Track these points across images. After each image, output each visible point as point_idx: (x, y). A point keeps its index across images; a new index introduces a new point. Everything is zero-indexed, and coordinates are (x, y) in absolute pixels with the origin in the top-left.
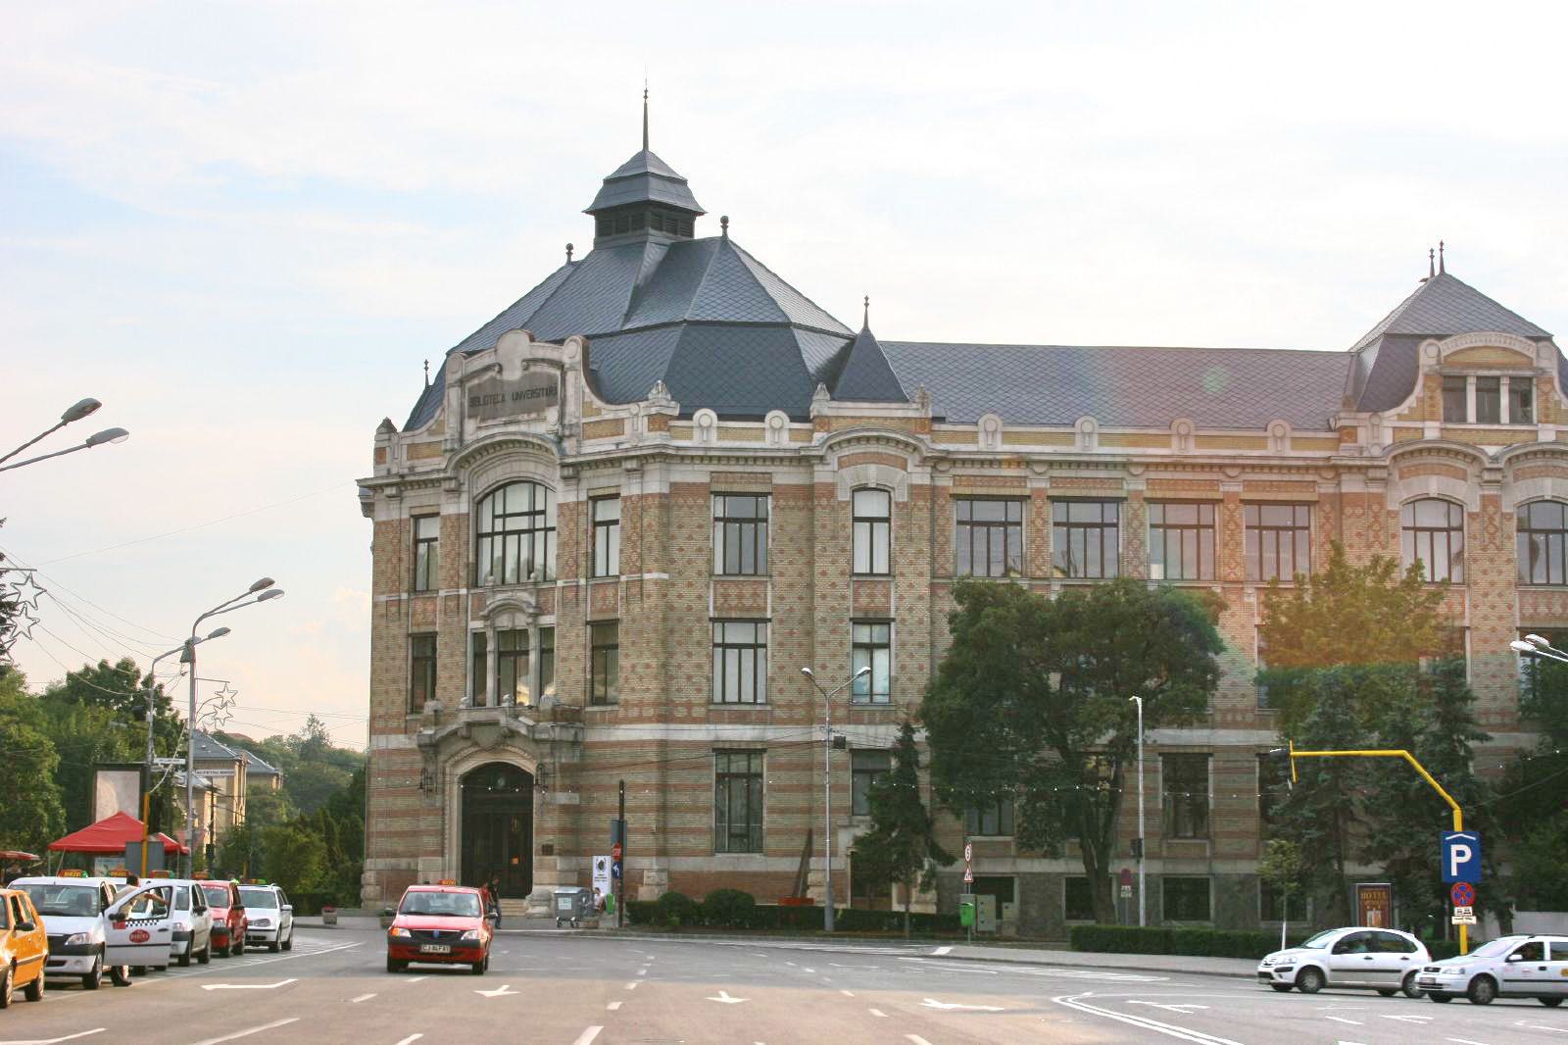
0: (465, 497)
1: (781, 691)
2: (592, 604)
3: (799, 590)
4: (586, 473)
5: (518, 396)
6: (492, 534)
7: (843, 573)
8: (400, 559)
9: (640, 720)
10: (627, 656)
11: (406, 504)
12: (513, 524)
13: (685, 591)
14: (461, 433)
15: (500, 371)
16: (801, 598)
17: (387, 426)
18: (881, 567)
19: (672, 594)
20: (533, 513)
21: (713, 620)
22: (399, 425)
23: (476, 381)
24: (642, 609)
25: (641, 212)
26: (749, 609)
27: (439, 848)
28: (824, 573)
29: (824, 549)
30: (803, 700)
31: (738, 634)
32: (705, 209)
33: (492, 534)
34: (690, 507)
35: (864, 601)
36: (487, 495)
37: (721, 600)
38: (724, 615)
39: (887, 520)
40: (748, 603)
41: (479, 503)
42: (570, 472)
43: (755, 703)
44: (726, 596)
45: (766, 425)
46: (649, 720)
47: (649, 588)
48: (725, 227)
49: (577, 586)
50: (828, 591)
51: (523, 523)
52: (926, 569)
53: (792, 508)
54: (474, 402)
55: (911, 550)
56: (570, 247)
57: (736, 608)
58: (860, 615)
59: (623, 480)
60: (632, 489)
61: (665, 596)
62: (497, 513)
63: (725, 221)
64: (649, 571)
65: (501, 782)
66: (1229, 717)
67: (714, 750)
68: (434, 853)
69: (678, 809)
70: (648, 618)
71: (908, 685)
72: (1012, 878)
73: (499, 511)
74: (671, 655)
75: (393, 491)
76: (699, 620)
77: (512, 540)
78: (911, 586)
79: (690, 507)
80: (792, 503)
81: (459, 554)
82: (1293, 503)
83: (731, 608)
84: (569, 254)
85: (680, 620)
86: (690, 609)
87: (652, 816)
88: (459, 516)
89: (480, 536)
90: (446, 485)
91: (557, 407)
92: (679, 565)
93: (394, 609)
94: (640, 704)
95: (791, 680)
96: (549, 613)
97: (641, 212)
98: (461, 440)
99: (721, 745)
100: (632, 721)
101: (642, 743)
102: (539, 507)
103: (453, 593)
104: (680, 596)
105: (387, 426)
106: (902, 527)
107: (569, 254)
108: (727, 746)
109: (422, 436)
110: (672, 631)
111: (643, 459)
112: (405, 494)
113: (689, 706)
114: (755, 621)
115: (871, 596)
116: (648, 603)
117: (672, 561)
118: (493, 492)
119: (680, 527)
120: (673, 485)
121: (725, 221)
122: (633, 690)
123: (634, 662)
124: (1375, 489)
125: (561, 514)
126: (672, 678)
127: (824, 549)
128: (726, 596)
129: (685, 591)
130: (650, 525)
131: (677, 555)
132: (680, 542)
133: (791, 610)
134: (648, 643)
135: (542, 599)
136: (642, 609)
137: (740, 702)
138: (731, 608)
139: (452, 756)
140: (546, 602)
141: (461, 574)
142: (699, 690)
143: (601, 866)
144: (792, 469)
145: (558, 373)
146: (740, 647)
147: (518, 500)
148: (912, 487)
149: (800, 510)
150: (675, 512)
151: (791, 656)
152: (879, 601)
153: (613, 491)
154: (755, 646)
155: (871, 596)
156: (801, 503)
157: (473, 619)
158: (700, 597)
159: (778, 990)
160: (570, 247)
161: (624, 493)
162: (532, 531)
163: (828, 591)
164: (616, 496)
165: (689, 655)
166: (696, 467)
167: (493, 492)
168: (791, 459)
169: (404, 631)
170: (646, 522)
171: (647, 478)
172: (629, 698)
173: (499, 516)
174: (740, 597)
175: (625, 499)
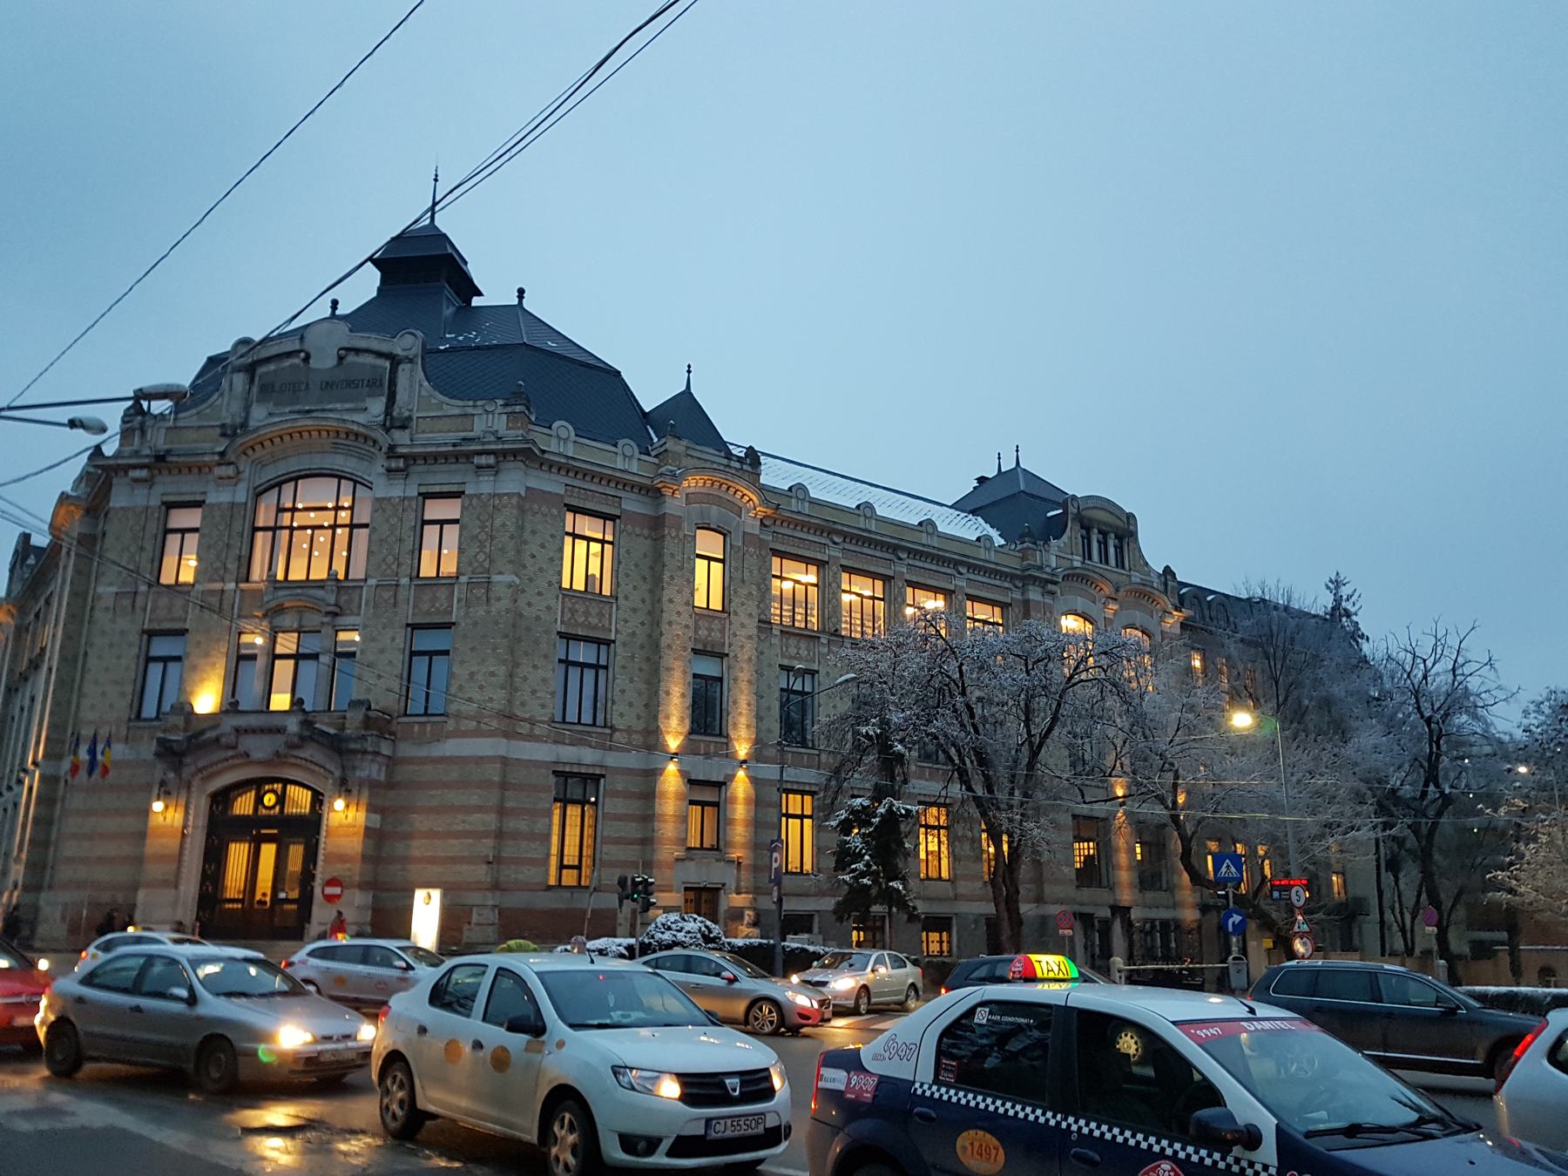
0: (242, 486)
1: (621, 715)
2: (415, 606)
4: (420, 468)
5: (328, 385)
8: (142, 548)
9: (531, 737)
10: (462, 662)
11: (158, 489)
13: (535, 600)
14: (247, 419)
15: (307, 359)
16: (643, 624)
19: (522, 603)
21: (561, 635)
23: (272, 367)
24: (488, 612)
25: (421, 268)
26: (595, 628)
27: (172, 878)
28: (671, 601)
29: (672, 578)
31: (582, 653)
34: (544, 515)
35: (703, 633)
37: (568, 616)
40: (594, 621)
41: (259, 494)
43: (594, 724)
44: (573, 611)
45: (618, 450)
46: (492, 734)
47: (498, 590)
52: (755, 612)
55: (743, 592)
57: (428, 613)
58: (700, 647)
59: (470, 478)
60: (485, 485)
63: (521, 292)
64: (500, 573)
65: (269, 799)
68: (165, 883)
69: (516, 835)
70: (497, 623)
72: (950, 919)
74: (516, 665)
75: (143, 473)
76: (547, 632)
78: (743, 625)
79: (544, 515)
80: (638, 530)
81: (228, 546)
83: (577, 624)
85: (528, 629)
86: (538, 618)
87: (489, 842)
88: (233, 505)
89: (255, 529)
91: (384, 399)
92: (531, 570)
93: (126, 602)
95: (631, 704)
96: (352, 614)
97: (421, 268)
98: (244, 425)
101: (480, 760)
103: (218, 586)
104: (529, 604)
106: (737, 569)
110: (519, 640)
111: (502, 455)
113: (532, 722)
114: (599, 642)
115: (710, 630)
116: (496, 607)
119: (533, 532)
121: (521, 292)
122: (470, 700)
123: (474, 669)
124: (1048, 600)
126: (517, 690)
127: (672, 578)
128: (573, 611)
129: (535, 600)
130: (504, 525)
131: (528, 561)
133: (634, 634)
134: (494, 650)
135: (344, 598)
136: (488, 612)
137: (579, 723)
138: (577, 624)
140: (349, 602)
141: (229, 566)
142: (543, 706)
144: (639, 497)
145: (388, 364)
146: (583, 666)
150: (529, 517)
151: (632, 681)
152: (716, 635)
153: (199, 498)
154: (596, 667)
156: (646, 532)
158: (549, 608)
165: (535, 667)
166: (553, 477)
167: (279, 485)
168: (641, 487)
169: (139, 628)
170: (498, 522)
171: (502, 476)
172: (463, 708)
174: (587, 614)
175: (471, 497)
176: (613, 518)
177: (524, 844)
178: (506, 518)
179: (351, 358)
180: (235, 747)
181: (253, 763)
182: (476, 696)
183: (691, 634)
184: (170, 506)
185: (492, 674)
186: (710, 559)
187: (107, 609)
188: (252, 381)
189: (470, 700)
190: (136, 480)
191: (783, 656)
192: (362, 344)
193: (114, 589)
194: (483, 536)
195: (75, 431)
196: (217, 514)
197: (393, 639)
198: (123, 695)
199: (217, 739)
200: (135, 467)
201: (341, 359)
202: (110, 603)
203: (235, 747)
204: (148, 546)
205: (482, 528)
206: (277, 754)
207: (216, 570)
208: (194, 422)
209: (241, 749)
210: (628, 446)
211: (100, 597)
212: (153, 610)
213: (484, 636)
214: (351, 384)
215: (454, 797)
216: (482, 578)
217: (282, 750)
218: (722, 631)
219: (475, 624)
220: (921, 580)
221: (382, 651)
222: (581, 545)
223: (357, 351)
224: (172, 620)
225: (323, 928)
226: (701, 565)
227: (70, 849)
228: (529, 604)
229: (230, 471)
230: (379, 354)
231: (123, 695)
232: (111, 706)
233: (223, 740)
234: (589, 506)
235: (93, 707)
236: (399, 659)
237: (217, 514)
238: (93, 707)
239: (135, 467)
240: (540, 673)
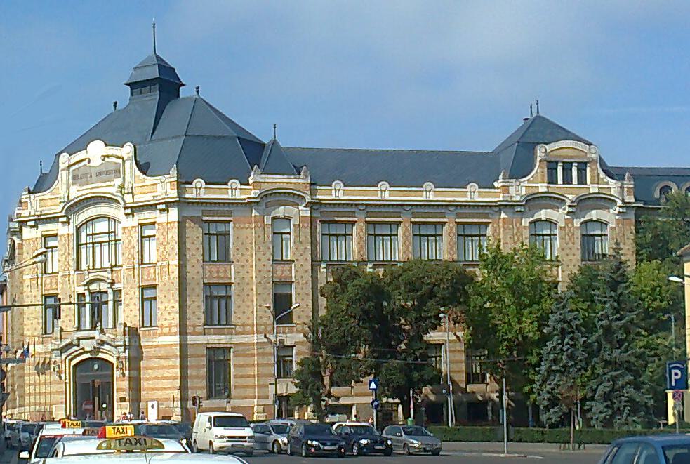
5: (99, 174)
23: (76, 166)
24: (169, 278)
26: (222, 278)
40: (222, 275)
42: (129, 211)
48: (198, 91)
54: (75, 178)
56: (116, 103)
73: (90, 232)
84: (115, 106)
93: (35, 282)
96: (118, 282)
100: (165, 335)
107: (115, 106)
118: (86, 223)
122: (166, 319)
143: (153, 406)
147: (102, 226)
153: (152, 221)
165: (193, 301)
173: (112, 232)
177: (195, 380)
179: (106, 159)
181: (87, 352)
182: (168, 317)
185: (173, 307)
187: (28, 286)
189: (166, 319)
190: (161, 210)
192: (110, 153)
193: (30, 277)
196: (63, 239)
197: (135, 293)
198: (39, 323)
199: (71, 343)
200: (30, 220)
201: (103, 160)
202: (29, 283)
203: (78, 346)
204: (559, 131)
206: (94, 348)
207: (66, 265)
208: (49, 196)
209: (81, 346)
212: (45, 285)
213: (169, 290)
214: (108, 172)
215: (163, 362)
217: (96, 346)
219: (165, 284)
220: (663, 457)
221: (131, 299)
223: (108, 156)
224: (53, 289)
225: (119, 418)
230: (117, 157)
231: (39, 323)
233: (74, 343)
235: (29, 329)
236: (138, 302)
237: (63, 239)
238: (29, 329)
239: (30, 220)
240: (196, 304)
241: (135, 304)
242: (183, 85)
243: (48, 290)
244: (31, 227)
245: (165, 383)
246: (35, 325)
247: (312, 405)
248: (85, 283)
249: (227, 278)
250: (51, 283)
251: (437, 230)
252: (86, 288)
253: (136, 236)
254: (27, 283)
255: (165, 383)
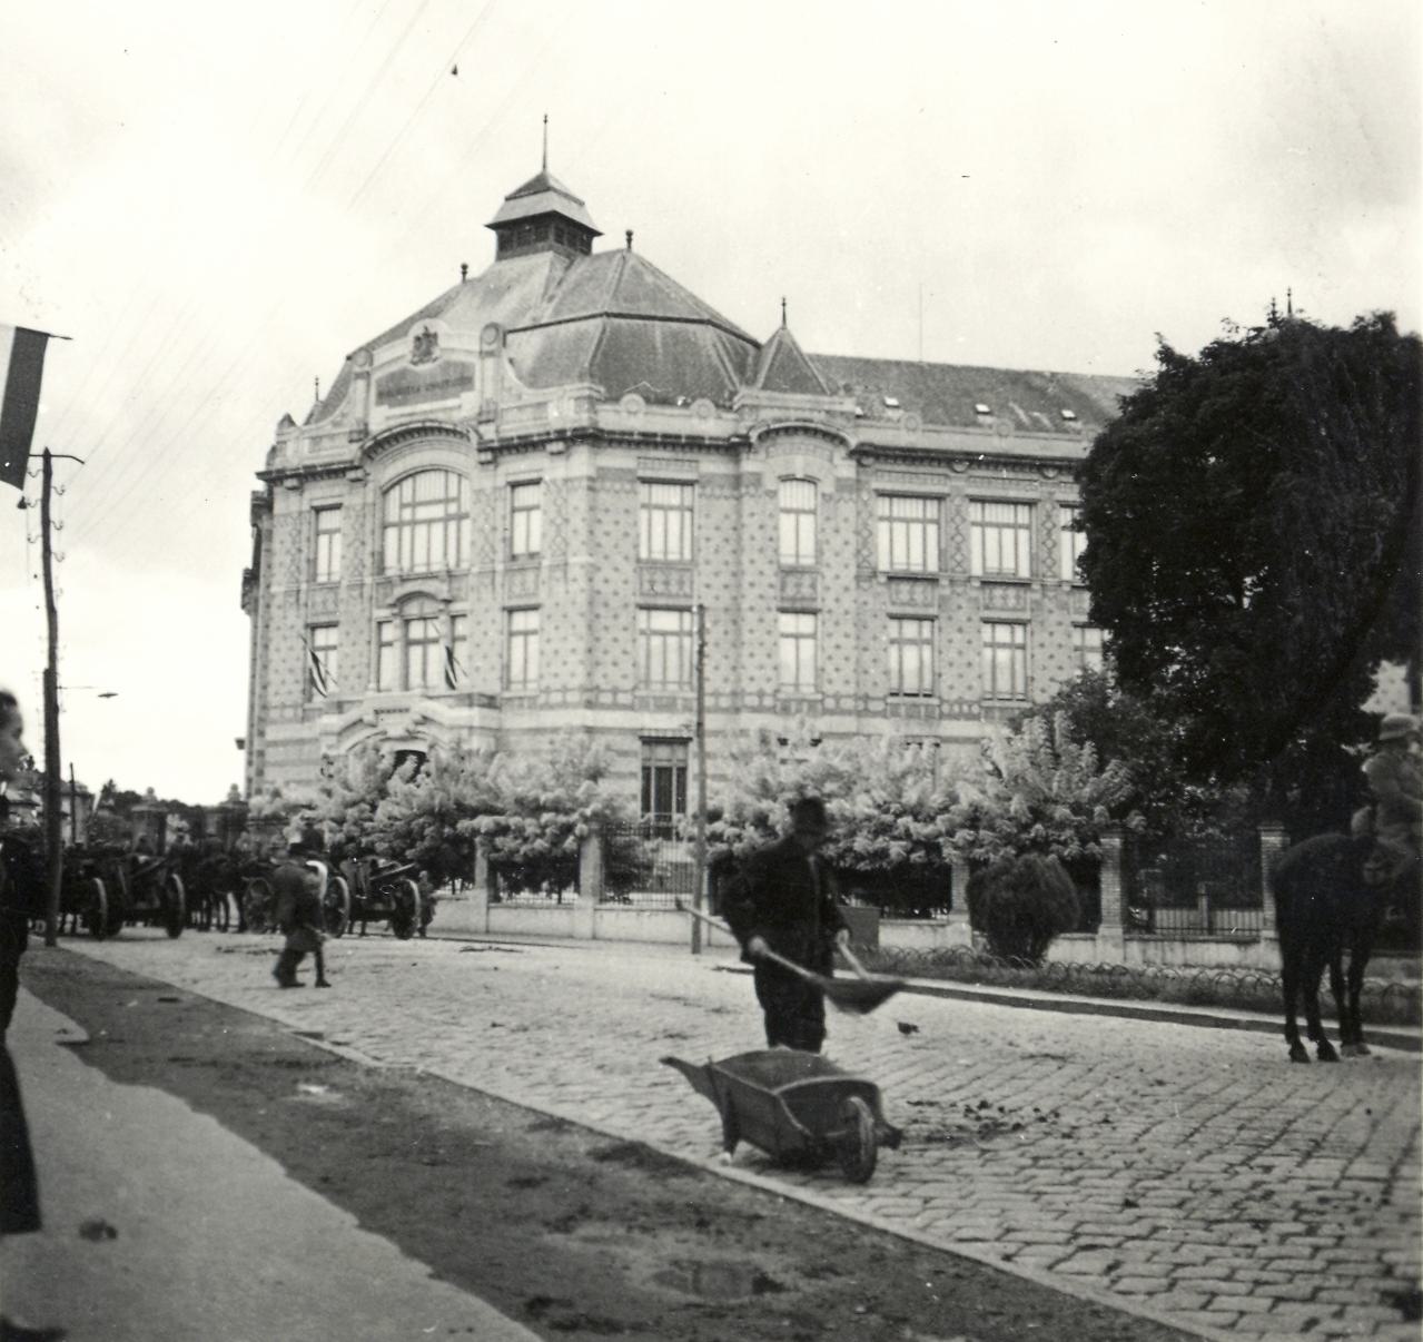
3: (726, 578)
6: (400, 525)
7: (771, 562)
9: (564, 705)
12: (422, 513)
17: (288, 420)
18: (687, 556)
19: (599, 577)
20: (447, 501)
22: (299, 419)
30: (728, 689)
32: (599, 228)
33: (400, 525)
35: (790, 591)
36: (392, 486)
38: (651, 601)
39: (813, 512)
40: (674, 588)
42: (488, 456)
48: (629, 240)
49: (494, 572)
50: (756, 579)
51: (422, 513)
53: (718, 498)
56: (464, 267)
57: (520, 596)
58: (787, 605)
61: (591, 580)
62: (405, 501)
63: (629, 234)
66: (956, 709)
67: (641, 738)
71: (834, 675)
73: (407, 498)
77: (421, 530)
82: (1015, 502)
83: (657, 594)
84: (464, 273)
89: (385, 527)
90: (352, 475)
94: (565, 690)
97: (541, 227)
99: (646, 734)
102: (453, 493)
105: (288, 420)
107: (464, 273)
108: (653, 734)
109: (326, 426)
112: (307, 486)
113: (615, 691)
117: (599, 545)
120: (600, 469)
121: (629, 234)
125: (477, 501)
131: (603, 540)
132: (608, 527)
138: (657, 594)
139: (301, 742)
147: (430, 486)
148: (838, 480)
149: (726, 498)
152: (806, 591)
153: (534, 476)
155: (798, 585)
156: (727, 492)
157: (379, 607)
159: (1198, 1029)
160: (464, 267)
161: (547, 478)
162: (447, 519)
163: (756, 579)
164: (536, 482)
173: (453, 500)
176: (690, 483)
178: (579, 499)
180: (374, 726)
183: (778, 593)
184: (318, 510)
186: (798, 512)
188: (368, 385)
190: (552, 454)
191: (893, 603)
193: (283, 589)
194: (559, 521)
195: (273, 427)
205: (559, 512)
210: (704, 405)
211: (273, 596)
216: (560, 560)
217: (412, 727)
218: (813, 586)
222: (658, 516)
226: (787, 522)
227: (1009, 565)
228: (606, 581)
229: (359, 474)
232: (970, 688)
234: (663, 474)
235: (277, 694)
238: (277, 694)
241: (493, 621)
242: (599, 234)
243: (316, 615)
244: (293, 489)
245: (658, 530)
246: (283, 646)
247: (1088, 743)
248: (390, 600)
249: (686, 596)
250: (324, 603)
251: (1008, 663)
252: (396, 611)
253: (502, 508)
254: (278, 601)
255: (658, 530)
